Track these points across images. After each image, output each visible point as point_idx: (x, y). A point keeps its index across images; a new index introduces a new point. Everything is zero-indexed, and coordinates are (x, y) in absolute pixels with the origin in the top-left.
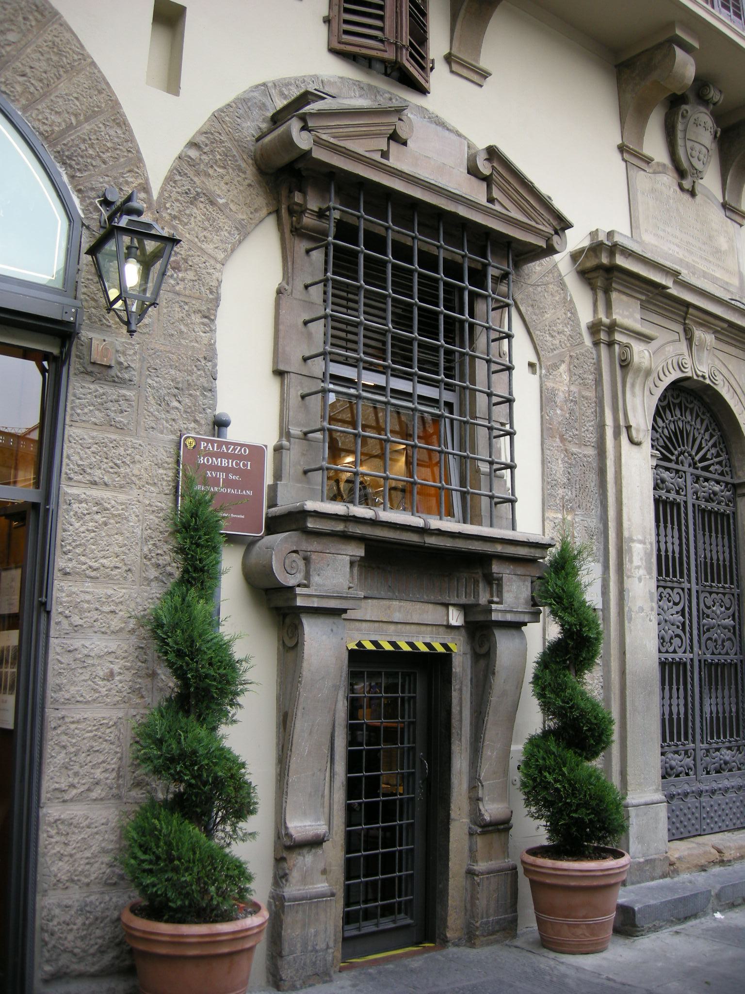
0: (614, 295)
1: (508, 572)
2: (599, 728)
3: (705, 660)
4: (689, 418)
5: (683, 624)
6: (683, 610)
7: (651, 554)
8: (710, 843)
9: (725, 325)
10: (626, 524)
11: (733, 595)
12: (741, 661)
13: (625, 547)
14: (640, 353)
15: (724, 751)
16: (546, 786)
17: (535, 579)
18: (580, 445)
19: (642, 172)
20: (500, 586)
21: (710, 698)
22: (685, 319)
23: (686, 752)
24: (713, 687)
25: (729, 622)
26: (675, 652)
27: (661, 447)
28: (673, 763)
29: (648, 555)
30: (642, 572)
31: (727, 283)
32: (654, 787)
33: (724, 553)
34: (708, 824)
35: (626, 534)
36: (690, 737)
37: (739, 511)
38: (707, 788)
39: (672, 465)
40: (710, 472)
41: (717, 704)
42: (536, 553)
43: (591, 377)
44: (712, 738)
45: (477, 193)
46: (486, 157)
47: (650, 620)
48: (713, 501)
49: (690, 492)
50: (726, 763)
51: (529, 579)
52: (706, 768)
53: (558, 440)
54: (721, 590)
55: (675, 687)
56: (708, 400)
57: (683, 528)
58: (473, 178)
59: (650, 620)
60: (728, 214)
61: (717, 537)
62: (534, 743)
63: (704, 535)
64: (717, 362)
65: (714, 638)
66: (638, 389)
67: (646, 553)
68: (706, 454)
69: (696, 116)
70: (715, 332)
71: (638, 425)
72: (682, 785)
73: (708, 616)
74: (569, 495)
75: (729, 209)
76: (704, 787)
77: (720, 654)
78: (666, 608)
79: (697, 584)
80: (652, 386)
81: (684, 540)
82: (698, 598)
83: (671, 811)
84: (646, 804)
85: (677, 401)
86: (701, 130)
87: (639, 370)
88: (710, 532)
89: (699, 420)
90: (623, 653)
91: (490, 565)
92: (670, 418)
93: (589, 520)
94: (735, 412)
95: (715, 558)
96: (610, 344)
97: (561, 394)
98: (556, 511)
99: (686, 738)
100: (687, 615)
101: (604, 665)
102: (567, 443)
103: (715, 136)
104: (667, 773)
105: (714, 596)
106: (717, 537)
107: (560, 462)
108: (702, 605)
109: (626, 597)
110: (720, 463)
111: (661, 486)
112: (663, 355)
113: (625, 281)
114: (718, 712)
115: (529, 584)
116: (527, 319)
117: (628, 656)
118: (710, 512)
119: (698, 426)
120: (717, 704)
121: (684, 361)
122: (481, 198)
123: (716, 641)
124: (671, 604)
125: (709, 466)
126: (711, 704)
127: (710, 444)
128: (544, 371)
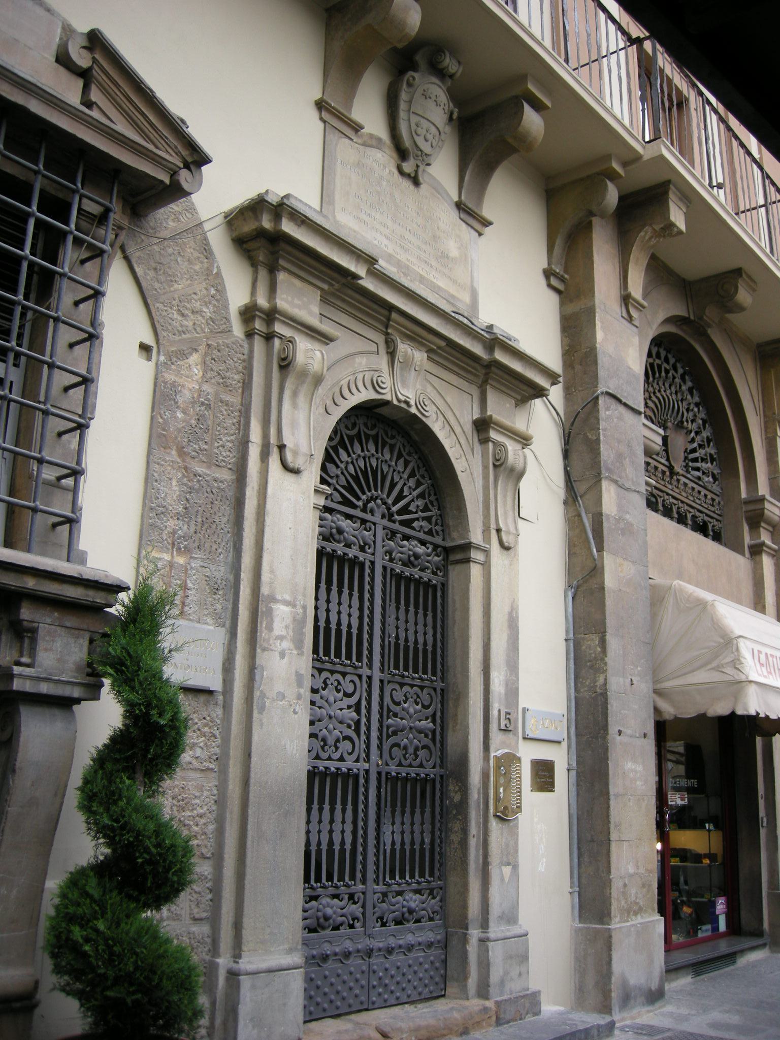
0: (282, 276)
1: (49, 620)
2: (164, 861)
3: (387, 773)
4: (387, 456)
5: (358, 723)
6: (358, 704)
7: (304, 621)
8: (374, 1023)
9: (443, 344)
10: (265, 576)
11: (435, 689)
12: (442, 776)
13: (262, 608)
14: (307, 352)
15: (325, 900)
16: (75, 948)
17: (97, 637)
18: (209, 465)
19: (347, 141)
20: (34, 641)
21: (393, 824)
22: (387, 328)
23: (351, 897)
24: (398, 809)
25: (427, 724)
26: (341, 759)
27: (343, 487)
28: (329, 911)
29: (299, 623)
30: (286, 645)
31: (453, 297)
32: (286, 946)
33: (425, 634)
34: (380, 994)
35: (265, 590)
36: (359, 875)
37: (450, 582)
38: (381, 945)
39: (357, 513)
40: (413, 529)
41: (403, 832)
42: (98, 598)
43: (237, 377)
44: (393, 877)
45: (70, 91)
46: (85, 43)
47: (295, 712)
48: (414, 566)
49: (380, 551)
50: (411, 911)
51: (87, 636)
52: (381, 918)
53: (174, 452)
54: (418, 682)
55: (339, 807)
56: (416, 438)
57: (367, 596)
58: (62, 70)
59: (295, 712)
60: (462, 216)
61: (416, 613)
62: (76, 880)
63: (398, 609)
64: (429, 389)
65: (402, 744)
66: (302, 400)
67: (294, 620)
68: (408, 504)
69: (426, 87)
70: (430, 351)
71: (297, 445)
72: (344, 942)
73: (396, 715)
74: (184, 529)
75: (465, 211)
76: (376, 944)
77: (410, 765)
78: (332, 699)
79: (382, 671)
80: (329, 402)
81: (366, 612)
82: (382, 690)
83: (309, 980)
84: (270, 971)
85: (373, 432)
86: (431, 104)
87: (303, 374)
88: (407, 605)
89: (401, 461)
90: (248, 755)
91: (18, 608)
92: (359, 452)
93: (213, 568)
94: (450, 454)
95: (411, 638)
96: (269, 337)
97: (186, 392)
98: (162, 550)
99: (353, 877)
100: (364, 711)
101: (220, 771)
102: (188, 459)
103: (451, 119)
104: (319, 925)
105: (406, 689)
106: (416, 613)
107: (174, 483)
108: (387, 700)
109: (257, 677)
110: (428, 519)
111: (337, 537)
112: (346, 368)
113: (298, 259)
114: (403, 843)
115: (86, 643)
116: (144, 284)
117: (254, 759)
118: (409, 580)
119: (400, 468)
120: (403, 832)
121: (380, 379)
122: (73, 97)
123: (405, 748)
124: (340, 695)
125: (413, 520)
126: (393, 833)
127: (415, 493)
128: (162, 358)
